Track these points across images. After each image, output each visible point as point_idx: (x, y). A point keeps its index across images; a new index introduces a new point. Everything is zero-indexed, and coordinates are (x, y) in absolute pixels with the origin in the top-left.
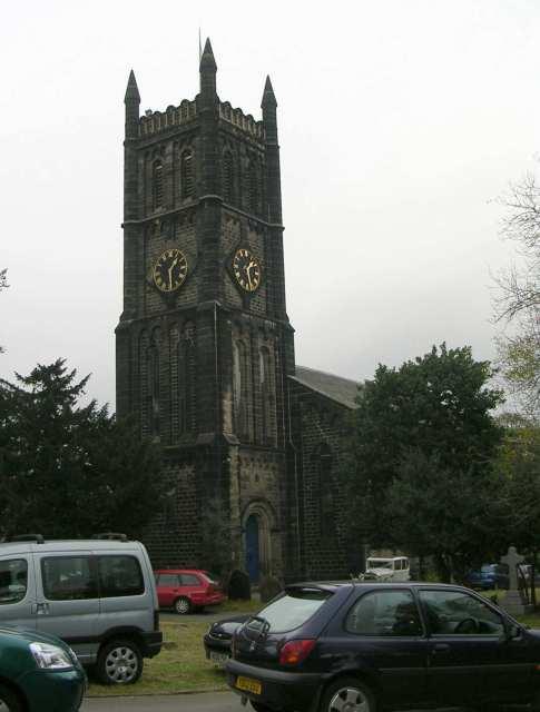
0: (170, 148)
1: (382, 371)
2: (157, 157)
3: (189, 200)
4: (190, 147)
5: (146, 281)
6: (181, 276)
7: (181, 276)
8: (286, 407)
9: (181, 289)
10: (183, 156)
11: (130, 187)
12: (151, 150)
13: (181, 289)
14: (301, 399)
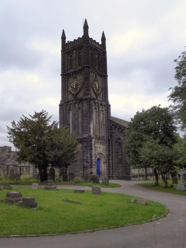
0: (75, 52)
3: (80, 67)
5: (68, 91)
6: (78, 89)
7: (78, 89)
9: (78, 93)
13: (78, 93)
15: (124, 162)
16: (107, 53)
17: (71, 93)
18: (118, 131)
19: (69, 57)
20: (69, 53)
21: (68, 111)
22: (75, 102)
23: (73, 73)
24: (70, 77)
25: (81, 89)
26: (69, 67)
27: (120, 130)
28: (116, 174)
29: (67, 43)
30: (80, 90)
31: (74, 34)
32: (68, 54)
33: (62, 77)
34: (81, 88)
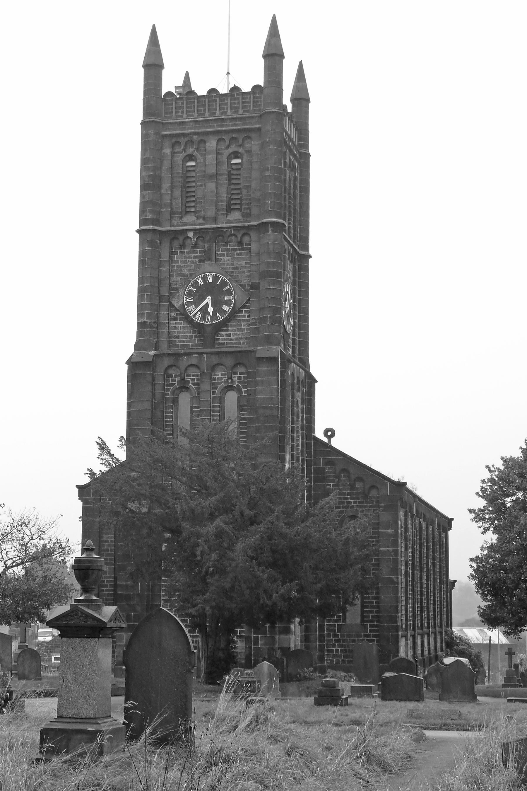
0: (212, 144)
1: (511, 457)
2: (190, 151)
3: (236, 215)
4: (241, 150)
5: (171, 305)
6: (225, 308)
7: (225, 308)
8: (309, 470)
9: (225, 323)
10: (229, 158)
11: (150, 185)
12: (183, 140)
13: (225, 323)
14: (330, 463)
15: (372, 612)
16: (312, 160)
17: (185, 317)
18: (352, 487)
19: (179, 159)
20: (183, 140)
21: (173, 393)
22: (215, 360)
23: (200, 233)
24: (182, 246)
25: (240, 311)
26: (178, 203)
27: (358, 485)
28: (334, 656)
29: (169, 94)
30: (234, 313)
31: (217, 63)
32: (177, 143)
33: (142, 243)
34: (239, 306)
